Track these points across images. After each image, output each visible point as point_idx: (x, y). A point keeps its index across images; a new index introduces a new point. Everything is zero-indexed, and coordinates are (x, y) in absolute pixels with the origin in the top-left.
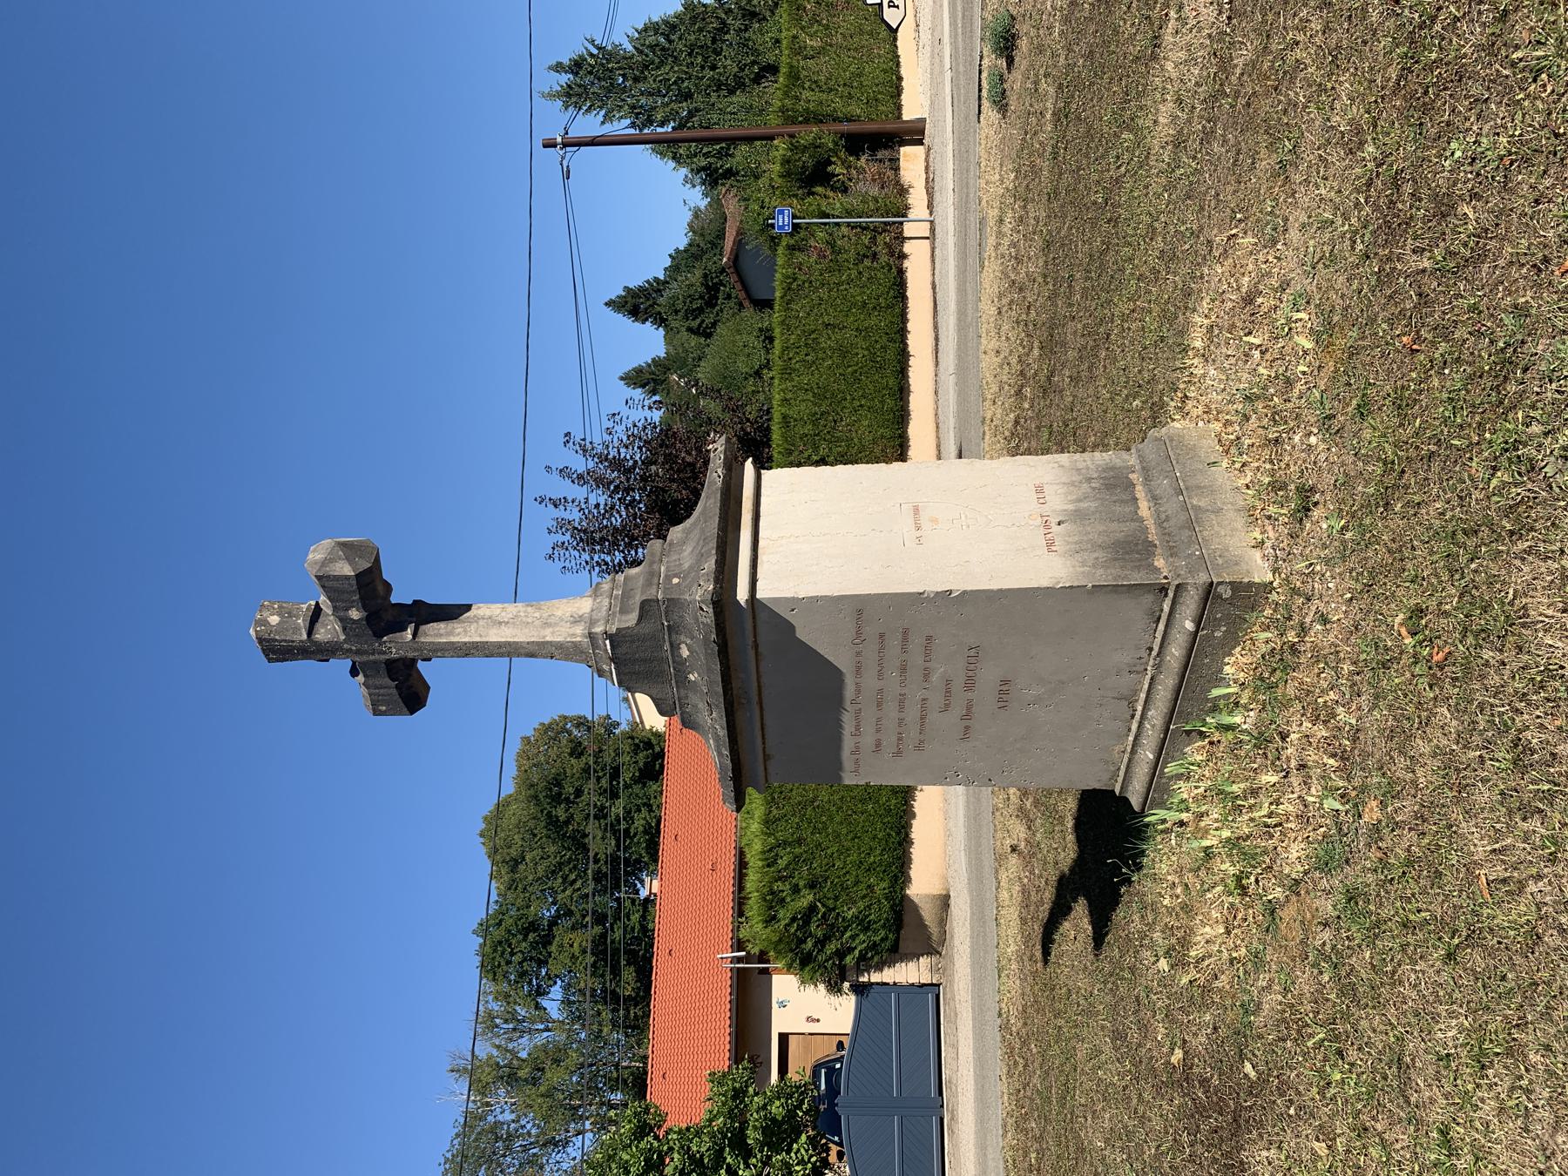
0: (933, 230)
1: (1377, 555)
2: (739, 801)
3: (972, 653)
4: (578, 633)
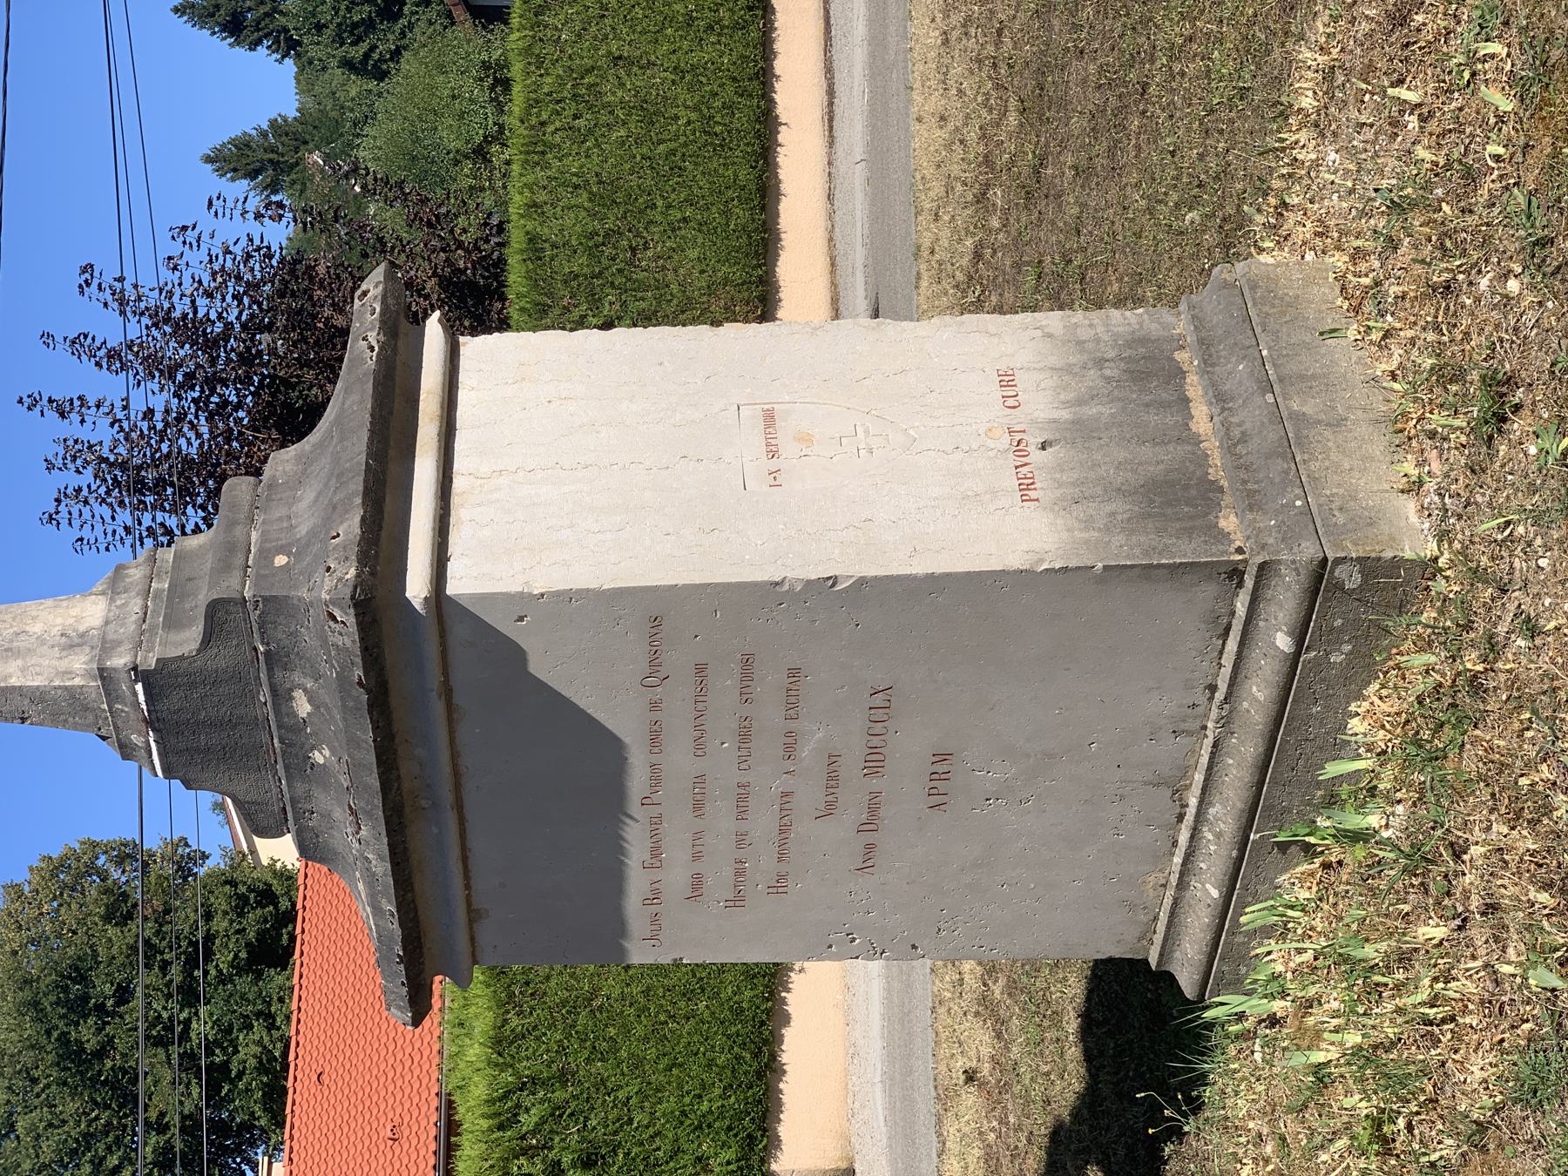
1: (301, 268)
2: (419, 1004)
3: (879, 700)
4: (77, 669)
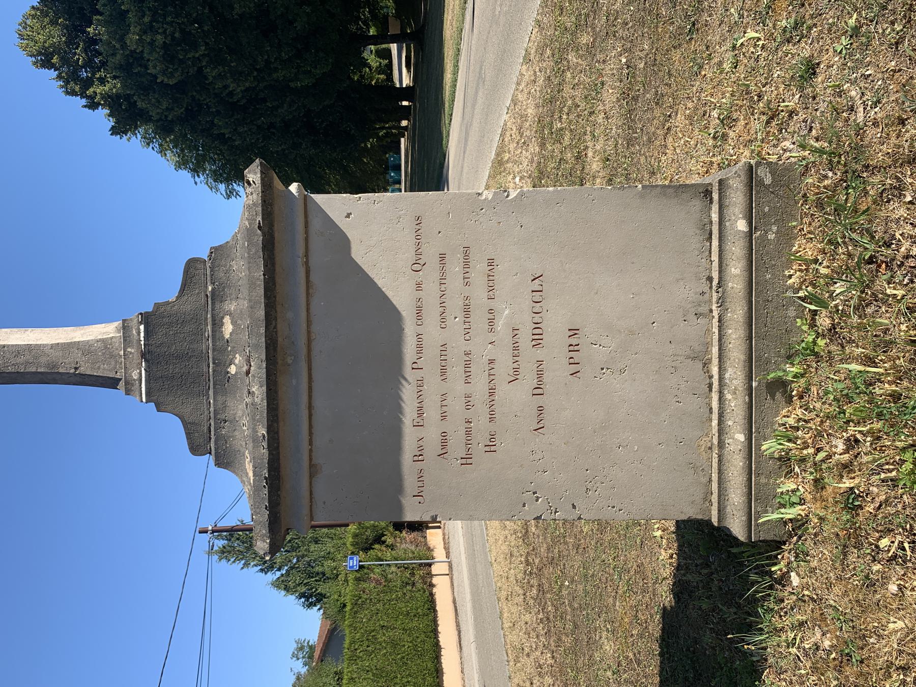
0: (451, 567)
3: (536, 285)
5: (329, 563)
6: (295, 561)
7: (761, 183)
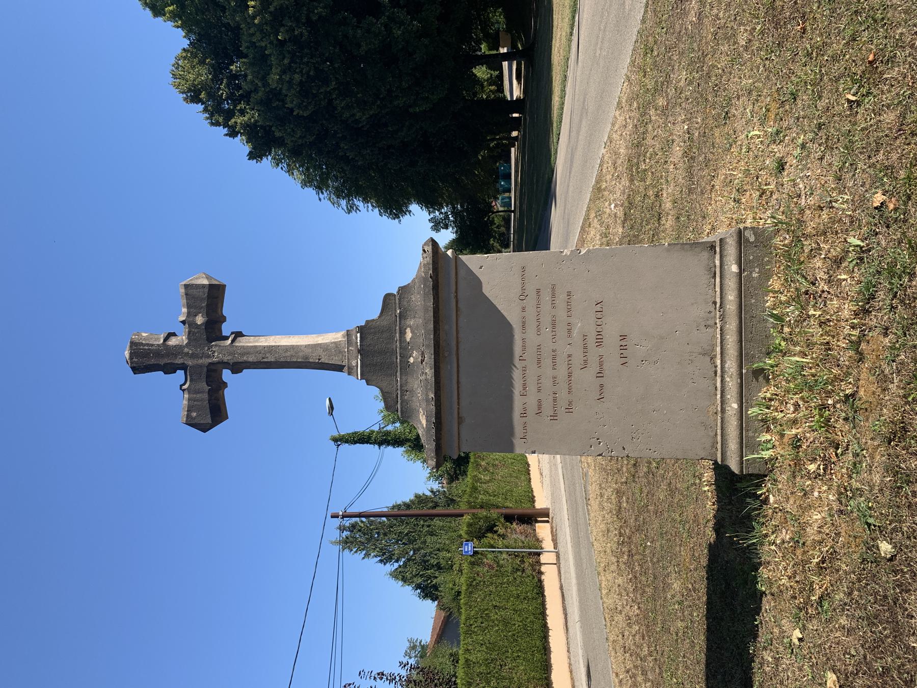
3: (598, 308)
5: (444, 554)
6: (412, 553)
7: (747, 240)
